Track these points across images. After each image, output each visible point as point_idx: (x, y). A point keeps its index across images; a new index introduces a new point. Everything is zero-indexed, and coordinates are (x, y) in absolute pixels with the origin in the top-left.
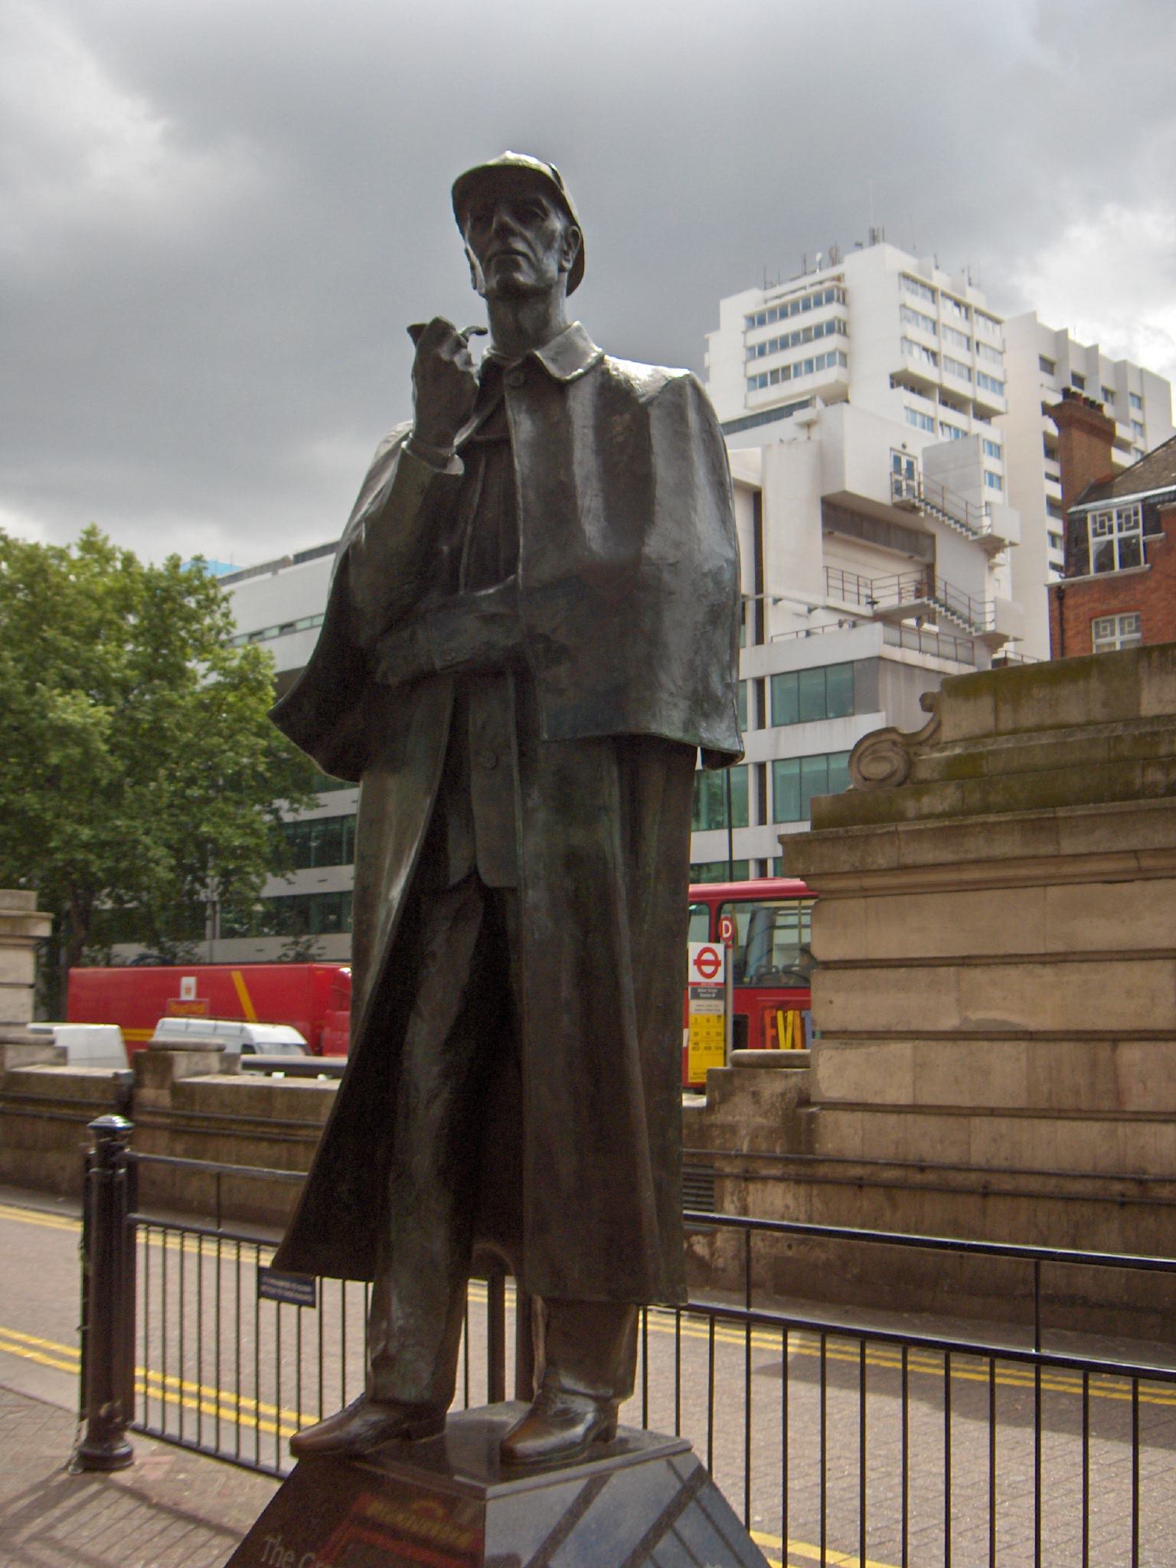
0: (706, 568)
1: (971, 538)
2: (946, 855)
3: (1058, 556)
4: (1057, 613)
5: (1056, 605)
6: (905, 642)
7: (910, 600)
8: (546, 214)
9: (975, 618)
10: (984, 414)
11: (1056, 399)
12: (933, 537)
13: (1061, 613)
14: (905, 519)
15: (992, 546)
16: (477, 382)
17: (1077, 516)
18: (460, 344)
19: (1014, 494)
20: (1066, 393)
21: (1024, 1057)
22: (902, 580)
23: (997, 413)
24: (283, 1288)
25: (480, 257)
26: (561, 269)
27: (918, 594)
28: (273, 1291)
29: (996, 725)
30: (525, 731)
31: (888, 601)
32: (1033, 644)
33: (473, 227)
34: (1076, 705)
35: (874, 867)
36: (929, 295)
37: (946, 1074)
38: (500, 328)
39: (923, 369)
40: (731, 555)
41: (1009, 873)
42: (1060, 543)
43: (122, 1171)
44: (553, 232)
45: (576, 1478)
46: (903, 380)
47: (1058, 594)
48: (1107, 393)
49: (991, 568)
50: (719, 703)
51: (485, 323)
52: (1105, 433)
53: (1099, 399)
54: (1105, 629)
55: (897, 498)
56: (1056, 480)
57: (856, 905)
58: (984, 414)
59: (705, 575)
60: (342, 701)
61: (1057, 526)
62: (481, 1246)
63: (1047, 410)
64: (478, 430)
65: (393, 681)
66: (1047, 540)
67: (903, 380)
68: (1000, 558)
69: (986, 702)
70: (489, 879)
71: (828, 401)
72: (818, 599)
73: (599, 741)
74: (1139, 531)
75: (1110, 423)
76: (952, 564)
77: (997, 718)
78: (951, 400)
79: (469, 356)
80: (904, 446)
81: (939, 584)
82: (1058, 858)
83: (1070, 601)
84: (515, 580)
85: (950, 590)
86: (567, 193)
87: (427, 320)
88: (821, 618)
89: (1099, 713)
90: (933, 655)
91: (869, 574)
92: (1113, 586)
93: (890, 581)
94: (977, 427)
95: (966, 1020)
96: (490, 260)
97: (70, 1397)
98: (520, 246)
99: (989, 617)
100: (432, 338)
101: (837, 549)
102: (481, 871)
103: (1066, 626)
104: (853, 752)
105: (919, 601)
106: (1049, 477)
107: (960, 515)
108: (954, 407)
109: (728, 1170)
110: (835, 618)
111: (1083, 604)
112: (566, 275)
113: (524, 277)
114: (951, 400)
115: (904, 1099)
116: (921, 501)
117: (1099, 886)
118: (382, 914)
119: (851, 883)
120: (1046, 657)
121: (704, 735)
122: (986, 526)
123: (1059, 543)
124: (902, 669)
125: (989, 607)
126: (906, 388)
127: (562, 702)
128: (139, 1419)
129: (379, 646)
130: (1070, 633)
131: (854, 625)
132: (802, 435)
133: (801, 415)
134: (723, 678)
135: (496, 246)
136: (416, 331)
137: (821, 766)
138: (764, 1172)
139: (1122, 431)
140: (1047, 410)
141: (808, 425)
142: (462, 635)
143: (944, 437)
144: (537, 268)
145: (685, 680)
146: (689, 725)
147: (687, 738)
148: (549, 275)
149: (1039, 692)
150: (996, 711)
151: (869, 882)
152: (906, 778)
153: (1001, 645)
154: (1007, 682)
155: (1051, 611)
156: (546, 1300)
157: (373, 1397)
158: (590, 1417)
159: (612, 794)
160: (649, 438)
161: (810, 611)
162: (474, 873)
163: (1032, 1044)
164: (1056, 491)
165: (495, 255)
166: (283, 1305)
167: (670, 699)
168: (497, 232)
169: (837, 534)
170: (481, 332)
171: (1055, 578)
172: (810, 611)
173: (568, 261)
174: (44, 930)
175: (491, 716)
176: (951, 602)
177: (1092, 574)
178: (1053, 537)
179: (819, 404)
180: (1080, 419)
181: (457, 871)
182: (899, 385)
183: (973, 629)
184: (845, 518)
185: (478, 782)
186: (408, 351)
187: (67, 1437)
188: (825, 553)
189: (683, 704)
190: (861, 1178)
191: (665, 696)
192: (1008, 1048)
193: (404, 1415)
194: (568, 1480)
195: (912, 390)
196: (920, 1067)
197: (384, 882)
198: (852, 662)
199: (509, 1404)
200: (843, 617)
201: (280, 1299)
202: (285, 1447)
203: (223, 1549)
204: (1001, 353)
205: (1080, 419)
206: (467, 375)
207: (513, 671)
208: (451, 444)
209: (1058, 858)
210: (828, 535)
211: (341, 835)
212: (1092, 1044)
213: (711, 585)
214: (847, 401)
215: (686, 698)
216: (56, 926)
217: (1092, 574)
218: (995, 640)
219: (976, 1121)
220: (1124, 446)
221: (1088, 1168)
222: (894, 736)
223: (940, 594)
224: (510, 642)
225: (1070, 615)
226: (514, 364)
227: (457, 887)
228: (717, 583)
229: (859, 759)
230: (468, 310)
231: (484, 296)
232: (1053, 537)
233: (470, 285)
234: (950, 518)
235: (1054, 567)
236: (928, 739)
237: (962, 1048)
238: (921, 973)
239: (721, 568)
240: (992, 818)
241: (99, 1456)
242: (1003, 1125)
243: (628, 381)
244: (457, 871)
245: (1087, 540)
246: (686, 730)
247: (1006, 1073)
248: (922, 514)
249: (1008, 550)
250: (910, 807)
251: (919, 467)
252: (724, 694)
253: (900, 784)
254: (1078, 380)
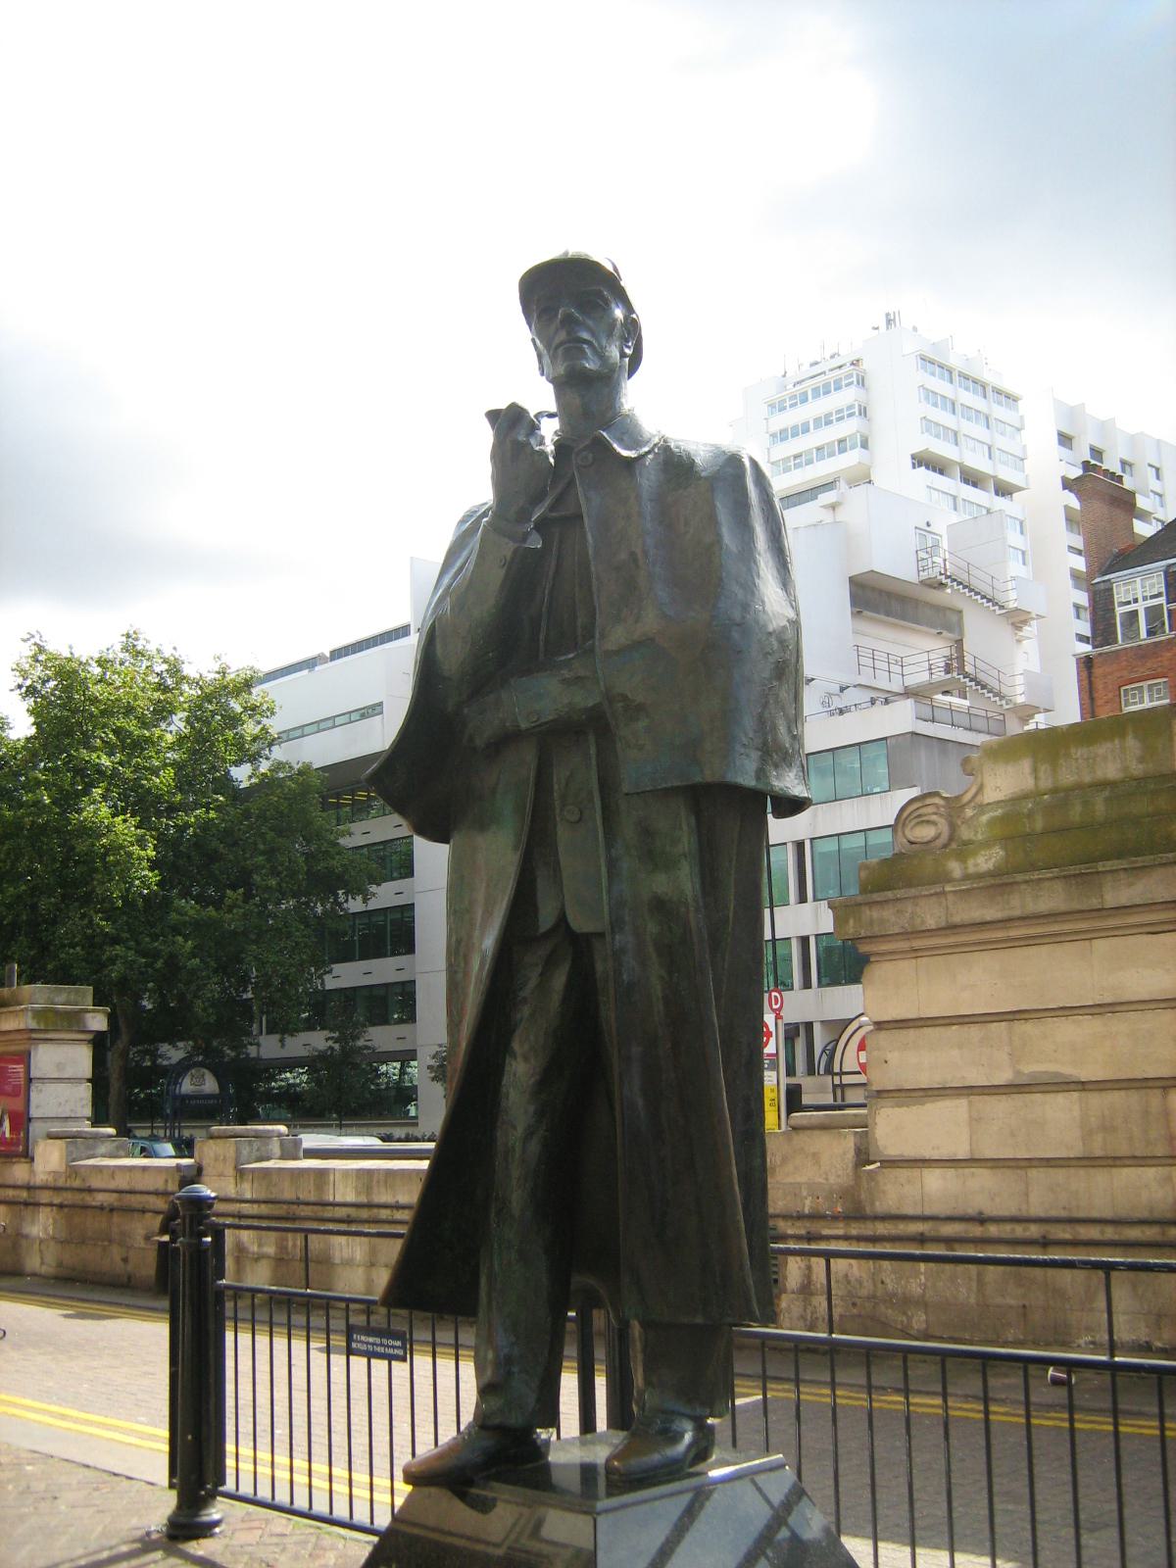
0: (771, 629)
1: (998, 612)
2: (991, 913)
3: (1086, 629)
4: (1085, 683)
5: (1085, 674)
6: (936, 718)
7: (940, 675)
8: (607, 303)
9: (1005, 690)
10: (1004, 490)
11: (1076, 472)
12: (961, 612)
13: (1090, 683)
14: (935, 596)
15: (1018, 619)
16: (552, 460)
17: (1102, 586)
18: (533, 428)
19: (1038, 565)
20: (1086, 465)
21: (1076, 1107)
22: (932, 656)
23: (1020, 489)
24: (373, 1344)
25: (548, 346)
26: (623, 355)
27: (948, 669)
28: (364, 1347)
29: (1036, 784)
30: (607, 785)
31: (918, 677)
32: (1068, 711)
33: (539, 317)
34: (1113, 762)
35: (924, 928)
36: (946, 374)
37: (1002, 1127)
38: (564, 411)
39: (944, 449)
40: (791, 615)
41: (1056, 928)
42: (1086, 615)
43: (209, 1239)
44: (615, 320)
45: (681, 1492)
46: (922, 461)
47: (1087, 664)
48: (1124, 463)
49: (1019, 641)
50: (787, 752)
51: (553, 409)
52: (1125, 503)
53: (1117, 469)
54: (1134, 696)
55: (924, 575)
56: (1079, 553)
57: (906, 966)
58: (1004, 490)
59: (770, 634)
60: (432, 765)
61: (1083, 598)
62: (579, 1280)
63: (1067, 484)
64: (552, 508)
65: (479, 742)
66: (1072, 611)
67: (922, 461)
68: (1027, 630)
69: (1026, 765)
70: (580, 923)
71: (853, 483)
72: (846, 680)
73: (668, 793)
74: (1162, 600)
75: (1132, 494)
76: (982, 637)
77: (1036, 778)
78: (972, 478)
79: (543, 438)
80: (928, 525)
81: (968, 658)
82: (1100, 911)
83: (1097, 671)
84: (594, 644)
85: (979, 664)
86: (626, 283)
87: (503, 406)
88: (853, 696)
89: (1137, 769)
90: (966, 729)
91: (898, 651)
92: (1143, 653)
93: (919, 655)
94: (1000, 503)
95: (1018, 1073)
96: (556, 348)
97: (160, 1472)
98: (585, 335)
99: (1020, 689)
100: (510, 423)
101: (864, 626)
102: (570, 918)
103: (1095, 695)
104: (893, 827)
105: (949, 676)
106: (1071, 548)
107: (988, 591)
108: (975, 485)
109: (790, 1232)
110: (867, 695)
111: (1111, 673)
112: (627, 360)
113: (591, 365)
114: (972, 478)
115: (962, 1153)
116: (947, 577)
117: (1145, 936)
118: (475, 964)
119: (904, 945)
120: (1077, 719)
121: (776, 783)
122: (1012, 600)
123: (1083, 614)
124: (935, 742)
125: (1020, 680)
126: (927, 468)
127: (641, 760)
128: (230, 1485)
129: (466, 711)
130: (1099, 702)
131: (887, 702)
132: (827, 517)
133: (827, 498)
134: (790, 731)
135: (562, 336)
136: (493, 416)
137: (858, 841)
138: (826, 1232)
139: (1142, 502)
140: (1067, 484)
141: (833, 507)
142: (545, 696)
143: (117, 1143)
144: (602, 356)
145: (755, 732)
146: (761, 774)
147: (760, 786)
148: (612, 361)
149: (1079, 752)
150: (1035, 770)
151: (917, 943)
152: (951, 839)
153: (1031, 716)
154: (1050, 744)
155: (1079, 681)
156: (643, 1324)
157: (482, 1421)
158: (688, 1437)
159: (686, 841)
160: (712, 506)
161: (842, 689)
162: (562, 919)
163: (1083, 1094)
164: (1080, 563)
165: (561, 344)
166: (373, 1361)
167: (742, 750)
168: (562, 322)
169: (866, 613)
170: (551, 416)
171: (1087, 648)
172: (842, 689)
173: (629, 347)
174: (98, 1022)
175: (575, 771)
176: (981, 676)
177: (1121, 643)
178: (1077, 607)
179: (842, 485)
180: (1102, 491)
181: (546, 918)
182: (920, 465)
183: (1004, 702)
184: (873, 597)
185: (563, 835)
186: (486, 436)
187: (165, 1504)
188: (855, 632)
189: (755, 755)
190: (922, 1234)
191: (738, 747)
192: (1061, 1100)
193: (499, 1453)
194: (672, 1495)
195: (934, 470)
196: (975, 1121)
197: (477, 933)
198: (885, 739)
199: (602, 1434)
200: (874, 695)
201: (370, 1355)
202: (399, 1474)
203: (362, 1547)
204: (1019, 430)
205: (1102, 491)
206: (543, 454)
207: (592, 728)
208: (530, 521)
209: (1100, 911)
210: (857, 614)
211: (385, 926)
212: (1143, 1092)
213: (775, 645)
214: (870, 482)
215: (757, 749)
216: (112, 1018)
217: (1121, 643)
218: (1026, 712)
219: (1033, 1173)
220: (1144, 516)
221: (1145, 1215)
222: (937, 800)
223: (968, 669)
224: (591, 703)
225: (1099, 685)
226: (581, 446)
227: (547, 935)
228: (782, 642)
229: (904, 825)
230: (539, 396)
231: (550, 382)
232: (1077, 607)
233: (538, 373)
234: (977, 594)
235: (1081, 638)
236: (970, 801)
237: (1018, 1100)
238: (974, 1032)
239: (784, 627)
240: (1036, 876)
241: (186, 1527)
242: (1060, 1175)
243: (689, 456)
244: (546, 918)
245: (1114, 609)
246: (758, 779)
247: (1059, 1123)
248: (949, 591)
249: (1034, 623)
250: (955, 868)
251: (945, 544)
252: (791, 745)
253: (945, 846)
254: (1097, 453)
